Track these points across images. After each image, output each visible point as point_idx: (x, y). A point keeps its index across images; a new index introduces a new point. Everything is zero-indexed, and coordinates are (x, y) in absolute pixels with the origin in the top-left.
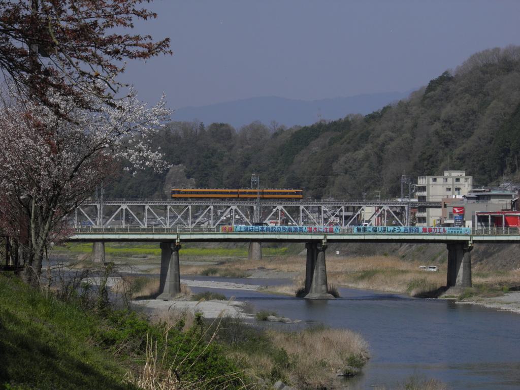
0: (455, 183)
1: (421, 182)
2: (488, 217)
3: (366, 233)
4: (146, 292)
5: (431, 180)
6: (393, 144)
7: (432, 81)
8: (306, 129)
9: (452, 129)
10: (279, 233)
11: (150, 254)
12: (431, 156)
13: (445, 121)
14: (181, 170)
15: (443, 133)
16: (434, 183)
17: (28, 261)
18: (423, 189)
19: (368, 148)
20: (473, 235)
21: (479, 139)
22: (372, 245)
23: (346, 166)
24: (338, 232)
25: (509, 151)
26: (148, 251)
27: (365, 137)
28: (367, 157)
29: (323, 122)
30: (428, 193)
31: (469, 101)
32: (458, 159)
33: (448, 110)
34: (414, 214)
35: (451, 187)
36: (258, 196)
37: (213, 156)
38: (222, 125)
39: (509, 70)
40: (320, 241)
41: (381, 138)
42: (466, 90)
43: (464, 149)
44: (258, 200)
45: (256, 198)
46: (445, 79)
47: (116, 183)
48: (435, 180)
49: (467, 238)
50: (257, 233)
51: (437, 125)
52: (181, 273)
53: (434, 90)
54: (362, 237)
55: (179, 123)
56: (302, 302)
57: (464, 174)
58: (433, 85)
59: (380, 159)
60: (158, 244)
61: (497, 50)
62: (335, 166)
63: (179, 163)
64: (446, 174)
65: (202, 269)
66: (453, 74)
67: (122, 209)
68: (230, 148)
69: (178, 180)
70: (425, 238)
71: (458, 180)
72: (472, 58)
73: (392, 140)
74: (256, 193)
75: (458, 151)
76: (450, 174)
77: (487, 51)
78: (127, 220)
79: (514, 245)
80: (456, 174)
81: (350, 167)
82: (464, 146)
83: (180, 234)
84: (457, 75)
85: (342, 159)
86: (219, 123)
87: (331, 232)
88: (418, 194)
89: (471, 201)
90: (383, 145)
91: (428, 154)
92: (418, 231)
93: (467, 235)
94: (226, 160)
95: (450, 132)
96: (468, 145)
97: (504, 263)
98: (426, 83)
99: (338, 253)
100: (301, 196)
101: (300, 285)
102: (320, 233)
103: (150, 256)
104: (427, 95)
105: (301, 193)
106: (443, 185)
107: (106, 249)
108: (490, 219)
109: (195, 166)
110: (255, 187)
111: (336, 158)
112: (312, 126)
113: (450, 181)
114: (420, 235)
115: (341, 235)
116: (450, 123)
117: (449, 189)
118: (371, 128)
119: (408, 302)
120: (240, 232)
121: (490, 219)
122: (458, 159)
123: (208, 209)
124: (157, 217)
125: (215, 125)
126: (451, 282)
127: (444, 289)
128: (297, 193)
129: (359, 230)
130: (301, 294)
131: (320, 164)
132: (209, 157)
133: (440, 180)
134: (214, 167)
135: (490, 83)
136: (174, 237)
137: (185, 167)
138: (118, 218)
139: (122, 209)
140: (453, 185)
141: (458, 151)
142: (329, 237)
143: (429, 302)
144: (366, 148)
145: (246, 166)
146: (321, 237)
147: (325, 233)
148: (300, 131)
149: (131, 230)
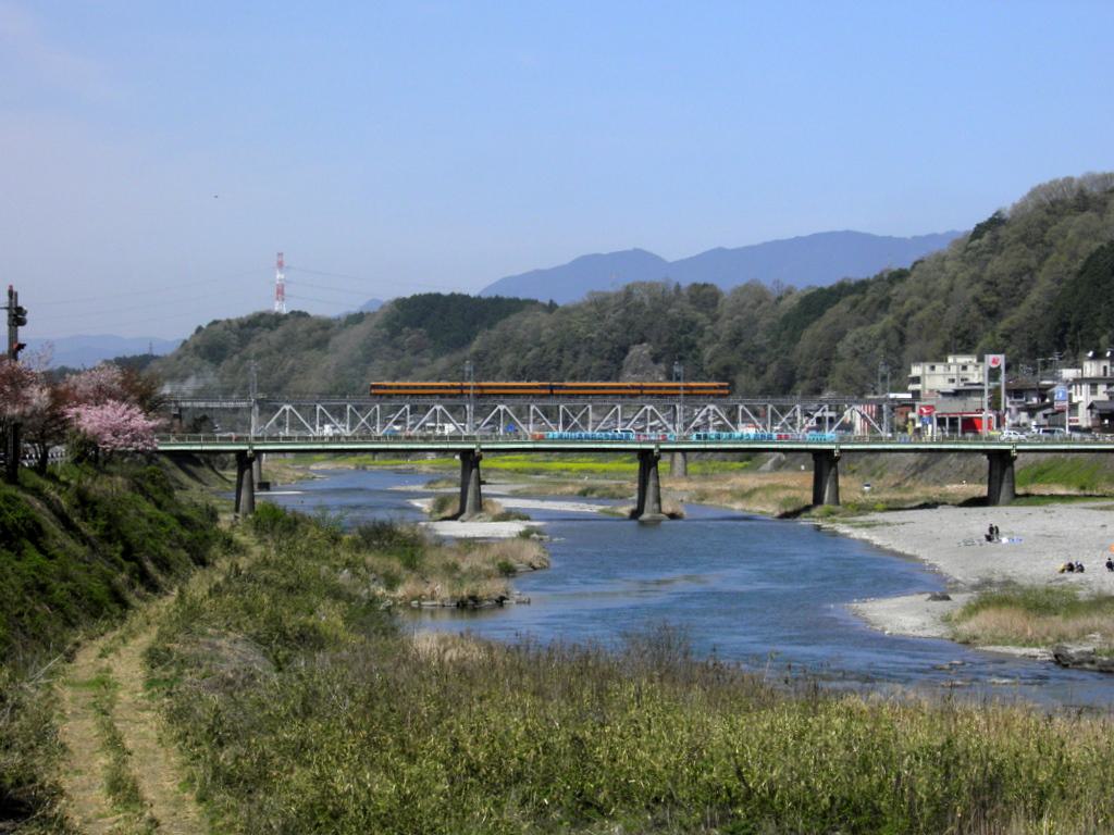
0: (961, 372)
1: (916, 371)
2: (957, 419)
3: (732, 441)
4: (448, 513)
5: (927, 368)
6: (920, 315)
7: (978, 226)
8: (821, 291)
9: (998, 294)
10: (601, 441)
11: (567, 470)
12: (967, 332)
13: (990, 283)
14: (645, 352)
15: (986, 299)
16: (933, 372)
17: (301, 474)
18: (917, 380)
19: (888, 320)
20: (840, 444)
21: (1033, 307)
22: (1103, 455)
23: (857, 347)
24: (673, 439)
25: (1068, 324)
26: (583, 466)
27: (884, 305)
28: (884, 335)
29: (846, 281)
30: (924, 387)
31: (1024, 253)
32: (1002, 336)
33: (999, 265)
34: (907, 414)
35: (955, 377)
36: (682, 392)
37: (691, 330)
38: (705, 285)
39: (1083, 209)
40: (651, 451)
41: (905, 307)
42: (1023, 239)
43: (1011, 322)
44: (682, 397)
45: (678, 395)
46: (996, 222)
47: (553, 370)
48: (933, 368)
49: (834, 447)
50: (574, 440)
51: (978, 288)
52: (483, 491)
53: (980, 237)
54: (702, 446)
55: (644, 283)
56: (634, 523)
57: (975, 360)
58: (979, 231)
59: (902, 339)
60: (635, 455)
61: (1069, 180)
62: (841, 347)
63: (642, 342)
64: (951, 360)
65: (579, 489)
66: (1007, 215)
67: (499, 410)
68: (715, 319)
69: (641, 366)
70: (780, 446)
71: (964, 368)
72: (1033, 193)
73: (920, 308)
74: (677, 388)
75: (1003, 325)
76: (955, 360)
77: (1055, 182)
78: (292, 426)
79: (952, 455)
80: (962, 360)
81: (862, 348)
82: (1013, 317)
83: (481, 443)
84: (1013, 217)
85: (850, 338)
86: (702, 283)
87: (665, 440)
88: (912, 387)
89: (947, 399)
90: (908, 315)
91: (963, 329)
92: (771, 438)
93: (832, 443)
94: (708, 336)
95: (995, 299)
96: (1016, 316)
97: (938, 478)
98: (971, 227)
99: (803, 467)
100: (727, 392)
101: (633, 506)
102: (651, 442)
103: (565, 474)
104: (970, 245)
105: (728, 388)
106: (944, 375)
107: (688, 466)
108: (960, 421)
109: (665, 345)
110: (678, 379)
111: (841, 335)
112: (831, 288)
113: (954, 369)
114: (774, 443)
115: (677, 443)
116: (996, 286)
117: (953, 381)
118: (894, 292)
119: (769, 524)
120: (553, 440)
121: (960, 421)
122: (1002, 336)
123: (495, 411)
124: (579, 416)
125: (695, 285)
126: (818, 499)
127: (807, 508)
128: (722, 387)
129: (699, 437)
130: (635, 514)
131: (821, 344)
132: (685, 333)
133: (940, 368)
134: (692, 346)
135: (1054, 228)
136: (474, 446)
137: (651, 347)
138: (280, 423)
139: (499, 410)
140: (958, 374)
141: (1003, 325)
142: (662, 447)
143: (789, 523)
144: (884, 321)
145: (736, 344)
146: (653, 446)
147: (657, 443)
148: (812, 295)
149: (363, 438)
